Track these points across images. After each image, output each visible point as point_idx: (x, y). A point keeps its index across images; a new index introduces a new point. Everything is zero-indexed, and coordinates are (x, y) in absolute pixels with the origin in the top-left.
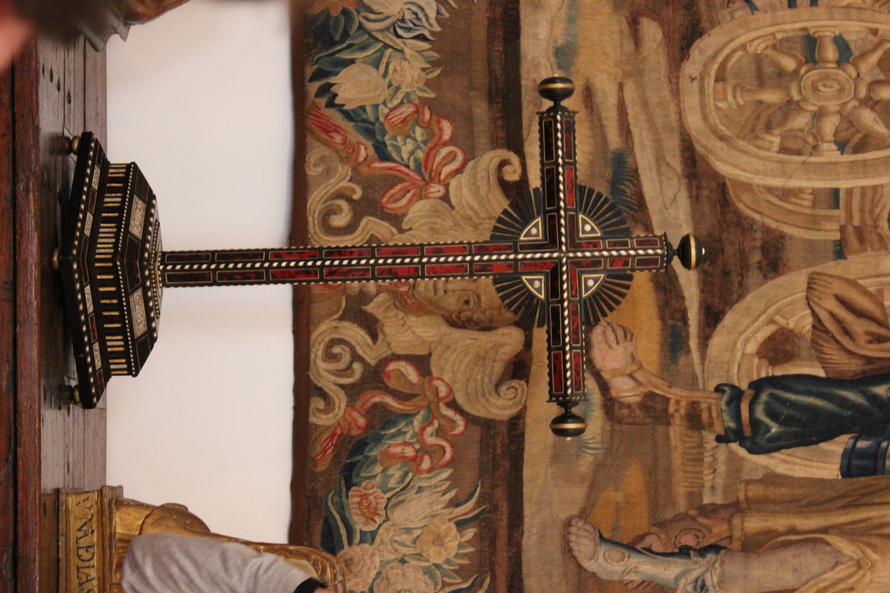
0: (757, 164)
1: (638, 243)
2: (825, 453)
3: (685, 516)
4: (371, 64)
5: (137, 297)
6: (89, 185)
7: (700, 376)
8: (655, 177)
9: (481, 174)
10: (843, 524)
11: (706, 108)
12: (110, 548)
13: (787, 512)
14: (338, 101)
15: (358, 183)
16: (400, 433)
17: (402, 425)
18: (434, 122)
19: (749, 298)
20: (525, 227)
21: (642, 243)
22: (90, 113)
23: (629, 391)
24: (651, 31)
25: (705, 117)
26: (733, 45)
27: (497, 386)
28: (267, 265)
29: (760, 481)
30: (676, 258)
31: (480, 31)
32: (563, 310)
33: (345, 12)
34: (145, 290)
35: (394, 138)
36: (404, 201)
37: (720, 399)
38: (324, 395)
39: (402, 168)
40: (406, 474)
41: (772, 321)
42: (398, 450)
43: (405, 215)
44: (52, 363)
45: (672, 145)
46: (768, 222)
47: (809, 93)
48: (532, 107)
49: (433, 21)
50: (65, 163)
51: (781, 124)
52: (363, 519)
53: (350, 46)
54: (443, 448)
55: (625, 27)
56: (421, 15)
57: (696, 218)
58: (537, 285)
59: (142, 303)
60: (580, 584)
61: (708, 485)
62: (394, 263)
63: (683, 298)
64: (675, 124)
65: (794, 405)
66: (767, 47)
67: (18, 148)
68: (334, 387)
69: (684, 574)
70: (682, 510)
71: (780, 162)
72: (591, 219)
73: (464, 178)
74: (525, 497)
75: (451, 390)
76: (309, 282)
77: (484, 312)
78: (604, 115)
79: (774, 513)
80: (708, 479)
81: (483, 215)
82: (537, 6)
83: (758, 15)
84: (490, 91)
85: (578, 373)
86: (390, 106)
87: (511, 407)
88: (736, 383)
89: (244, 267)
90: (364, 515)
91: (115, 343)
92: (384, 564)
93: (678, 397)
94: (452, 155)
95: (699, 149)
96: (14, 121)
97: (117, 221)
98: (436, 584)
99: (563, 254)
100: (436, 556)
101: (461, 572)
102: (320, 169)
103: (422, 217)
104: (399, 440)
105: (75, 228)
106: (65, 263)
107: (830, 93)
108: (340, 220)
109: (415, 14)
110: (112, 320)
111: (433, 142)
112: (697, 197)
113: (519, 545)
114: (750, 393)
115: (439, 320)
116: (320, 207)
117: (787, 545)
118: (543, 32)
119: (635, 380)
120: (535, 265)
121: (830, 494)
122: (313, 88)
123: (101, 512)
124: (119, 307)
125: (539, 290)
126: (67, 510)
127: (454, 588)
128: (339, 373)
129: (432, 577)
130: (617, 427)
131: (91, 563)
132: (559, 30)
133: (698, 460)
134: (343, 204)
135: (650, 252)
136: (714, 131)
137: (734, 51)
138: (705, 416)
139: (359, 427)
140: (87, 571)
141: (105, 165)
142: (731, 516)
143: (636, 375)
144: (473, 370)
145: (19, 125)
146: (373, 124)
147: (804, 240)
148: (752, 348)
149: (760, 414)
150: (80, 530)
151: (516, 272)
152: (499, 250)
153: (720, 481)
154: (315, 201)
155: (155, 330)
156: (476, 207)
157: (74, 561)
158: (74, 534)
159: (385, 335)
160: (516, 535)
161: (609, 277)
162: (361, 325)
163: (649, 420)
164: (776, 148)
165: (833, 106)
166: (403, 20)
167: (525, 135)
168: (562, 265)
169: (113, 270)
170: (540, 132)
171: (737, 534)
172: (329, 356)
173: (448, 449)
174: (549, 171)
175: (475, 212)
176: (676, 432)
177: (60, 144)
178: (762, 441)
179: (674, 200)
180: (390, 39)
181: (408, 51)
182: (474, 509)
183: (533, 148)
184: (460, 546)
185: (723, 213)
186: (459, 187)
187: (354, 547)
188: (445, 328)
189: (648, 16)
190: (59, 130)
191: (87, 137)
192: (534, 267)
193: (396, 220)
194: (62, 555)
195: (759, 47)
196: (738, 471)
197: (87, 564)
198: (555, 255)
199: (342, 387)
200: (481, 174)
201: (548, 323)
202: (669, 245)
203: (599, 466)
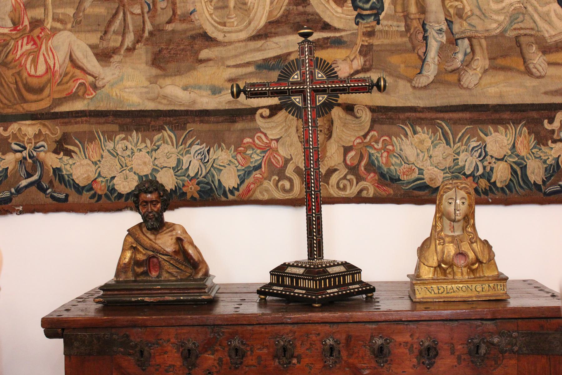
0: (260, 8)
1: (302, 54)
3: (410, 39)
4: (220, 173)
5: (330, 270)
6: (282, 291)
7: (352, 32)
9: (266, 125)
11: (237, 31)
12: (438, 280)
14: (236, 187)
15: (271, 177)
16: (377, 159)
17: (374, 158)
18: (244, 146)
19: (318, 11)
20: (295, 104)
23: (358, 62)
25: (241, 31)
27: (357, 118)
28: (314, 215)
29: (395, 7)
30: (308, 39)
32: (332, 87)
33: (198, 184)
34: (326, 267)
35: (252, 162)
36: (279, 158)
37: (362, 23)
39: (265, 159)
40: (395, 156)
42: (384, 159)
43: (285, 157)
44: (357, 306)
45: (253, 45)
46: (285, 3)
48: (244, 102)
50: (271, 301)
53: (213, 182)
54: (383, 140)
55: (203, 65)
56: (199, 152)
57: (285, 34)
58: (321, 99)
59: (332, 268)
60: (439, 82)
61: (397, 29)
62: (313, 160)
63: (318, 39)
64: (244, 44)
66: (211, 5)
67: (272, 322)
68: (358, 186)
69: (435, 39)
70: (408, 39)
72: (291, 76)
73: (268, 133)
74: (403, 105)
75: (359, 137)
76: (321, 197)
77: (325, 124)
80: (395, 29)
81: (284, 124)
83: (197, 9)
85: (359, 81)
87: (366, 112)
88: (355, 16)
89: (315, 225)
90: (411, 174)
91: (349, 279)
92: (432, 165)
93: (360, 41)
94: (259, 138)
95: (254, 34)
96: (259, 324)
98: (440, 143)
101: (434, 133)
102: (265, 194)
104: (380, 159)
105: (303, 297)
106: (319, 301)
108: (287, 185)
109: (198, 154)
110: (339, 281)
112: (274, 34)
113: (423, 108)
115: (329, 142)
116: (281, 193)
118: (205, 100)
119: (354, 59)
120: (313, 99)
122: (230, 197)
123: (424, 284)
124: (334, 278)
126: (423, 298)
127: (441, 135)
128: (351, 185)
129: (437, 145)
130: (374, 67)
131: (445, 288)
132: (204, 93)
133: (387, 32)
134: (280, 183)
135: (306, 49)
136: (246, 27)
137: (213, 19)
138: (369, 29)
139: (375, 176)
140: (448, 290)
141: (271, 284)
142: (410, 18)
143: (351, 59)
144: (350, 128)
145: (261, 322)
146: (246, 172)
148: (339, 10)
149: (368, 6)
150: (431, 293)
151: (315, 108)
152: (307, 114)
153: (395, 23)
155: (342, 262)
156: (281, 127)
157: (444, 294)
158: (433, 295)
160: (419, 109)
161: (317, 68)
162: (331, 176)
163: (371, 53)
168: (313, 88)
169: (320, 281)
171: (417, 16)
172: (344, 189)
173: (384, 138)
175: (283, 127)
176: (375, 41)
177: (263, 304)
178: (378, 6)
179: (277, 43)
180: (209, 165)
181: (214, 158)
182: (409, 128)
183: (255, 102)
184: (424, 133)
185: (282, 22)
187: (425, 177)
188: (332, 140)
189: (198, 56)
190: (256, 304)
191: (259, 292)
192: (313, 100)
193: (287, 161)
195: (211, 9)
197: (445, 289)
198: (308, 90)
199: (357, 183)
201: (334, 93)
202: (303, 42)
203: (391, 74)
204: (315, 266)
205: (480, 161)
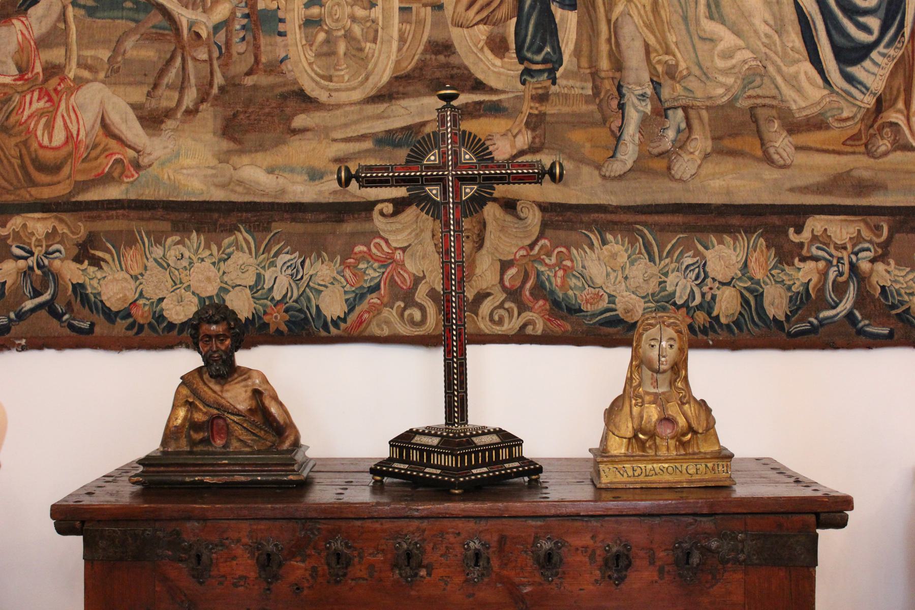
0: (383, 56)
1: (443, 125)
2: (562, 19)
5: (477, 440)
6: (406, 470)
8: (391, 120)
9: (388, 227)
10: (605, 10)
11: (348, 88)
13: (597, 44)
14: (342, 316)
15: (394, 303)
16: (548, 279)
19: (466, 63)
21: (442, 121)
22: (353, 468)
24: (299, 121)
25: (354, 89)
26: (309, 71)
27: (521, 219)
29: (578, 60)
31: (299, 228)
33: (286, 311)
35: (366, 281)
36: (405, 275)
37: (530, 82)
38: (524, 326)
40: (574, 275)
41: (482, 49)
42: (559, 280)
43: (414, 275)
44: (516, 493)
45: (371, 109)
47: (340, 24)
49: (293, 257)
51: (359, 42)
52: (601, 302)
53: (308, 308)
54: (558, 253)
55: (297, 137)
56: (289, 264)
57: (418, 94)
58: (469, 190)
60: (640, 170)
62: (455, 280)
63: (467, 104)
64: (358, 107)
65: (534, 37)
67: (391, 515)
70: (596, 107)
71: (382, 43)
73: (391, 238)
74: (587, 202)
75: (522, 248)
78: (352, 151)
79: (598, 52)
80: (577, 91)
82: (283, 191)
84: (336, 221)
85: (524, 166)
86: (345, 283)
87: (534, 211)
89: (457, 374)
91: (504, 454)
92: (627, 289)
93: (528, 107)
96: (372, 518)
97: (429, 453)
98: (640, 258)
99: (450, 173)
100: (623, 258)
101: (632, 243)
102: (385, 327)
103: (416, 264)
104: (553, 280)
105: (436, 479)
106: (460, 485)
107: (339, 10)
108: (417, 315)
109: (288, 267)
110: (490, 456)
111: (368, 257)
112: (403, 94)
113: (617, 207)
114: (526, 64)
116: (408, 327)
117: (618, 44)
118: (299, 188)
119: (517, 134)
121: (586, 17)
122: (334, 331)
123: (613, 462)
124: (483, 452)
125: (472, 189)
126: (610, 483)
128: (511, 316)
129: (635, 260)
130: (546, 145)
132: (299, 178)
133: (566, 96)
134: (407, 313)
136: (362, 83)
137: (313, 70)
138: (540, 92)
141: (391, 460)
146: (356, 295)
147: (431, 29)
148: (498, 62)
149: (539, 58)
152: (447, 214)
153: (578, 84)
154: (404, 330)
155: (495, 429)
156: (409, 230)
157: (642, 478)
158: (625, 479)
159: (487, 288)
161: (463, 145)
162: (481, 303)
164: (374, 45)
165: (348, 10)
166: (292, 275)
167: (362, 200)
169: (462, 455)
170: (371, 187)
171: (611, 74)
172: (500, 322)
173: (559, 249)
174: (397, 181)
175: (412, 231)
176: (549, 109)
177: (378, 488)
178: (555, 58)
179: (406, 108)
181: (311, 273)
182: (595, 235)
183: (373, 193)
184: (617, 243)
185: (414, 78)
186: (397, 241)
188: (484, 251)
189: (290, 123)
190: (368, 489)
191: (373, 471)
192: (457, 192)
193: (417, 280)
194: (638, 486)
195: (311, 55)
196: (572, 72)
199: (519, 314)
200: (388, 227)
201: (489, 182)
202: (444, 107)
203: (570, 157)
204: (456, 434)
205: (697, 285)
